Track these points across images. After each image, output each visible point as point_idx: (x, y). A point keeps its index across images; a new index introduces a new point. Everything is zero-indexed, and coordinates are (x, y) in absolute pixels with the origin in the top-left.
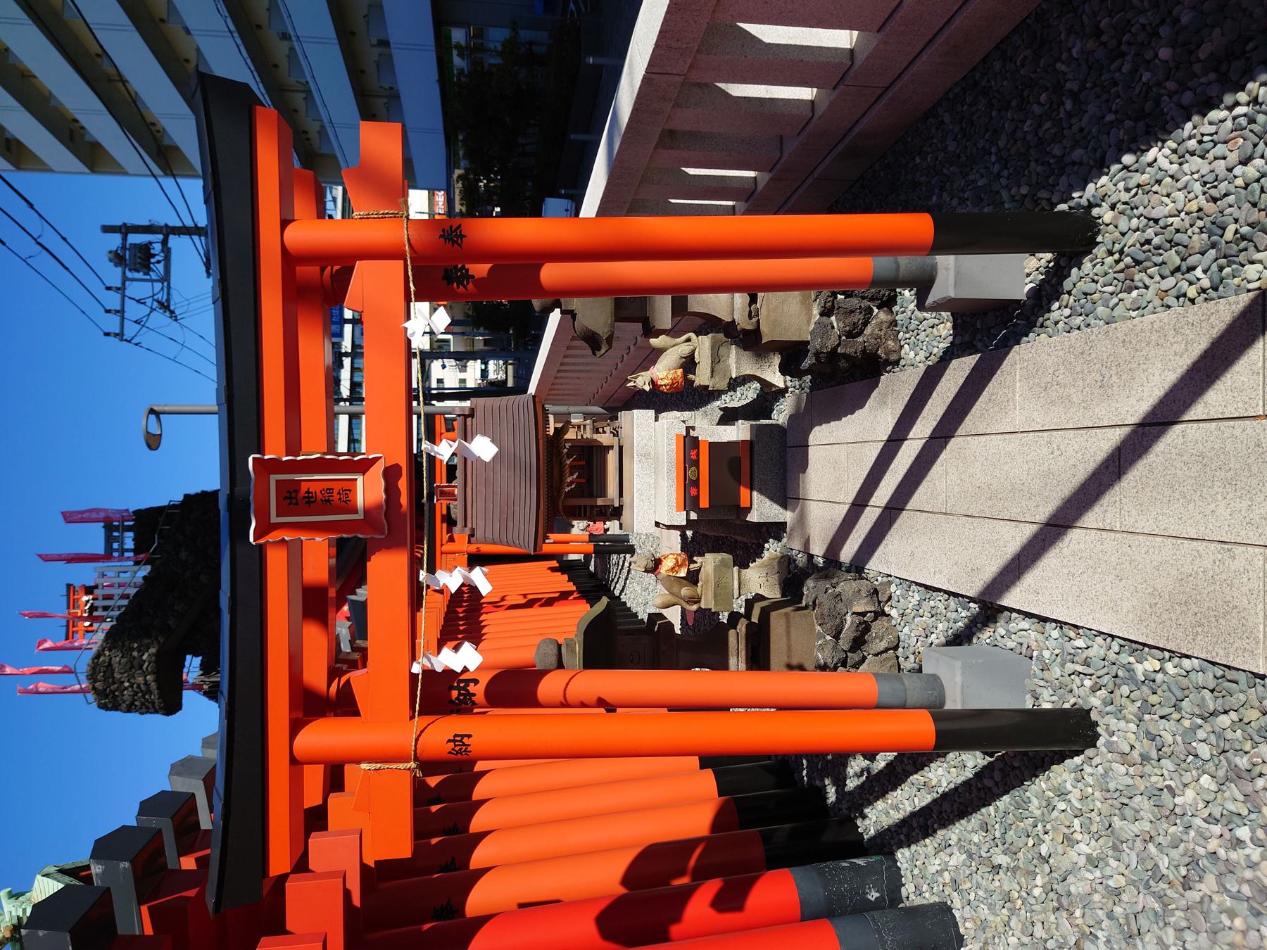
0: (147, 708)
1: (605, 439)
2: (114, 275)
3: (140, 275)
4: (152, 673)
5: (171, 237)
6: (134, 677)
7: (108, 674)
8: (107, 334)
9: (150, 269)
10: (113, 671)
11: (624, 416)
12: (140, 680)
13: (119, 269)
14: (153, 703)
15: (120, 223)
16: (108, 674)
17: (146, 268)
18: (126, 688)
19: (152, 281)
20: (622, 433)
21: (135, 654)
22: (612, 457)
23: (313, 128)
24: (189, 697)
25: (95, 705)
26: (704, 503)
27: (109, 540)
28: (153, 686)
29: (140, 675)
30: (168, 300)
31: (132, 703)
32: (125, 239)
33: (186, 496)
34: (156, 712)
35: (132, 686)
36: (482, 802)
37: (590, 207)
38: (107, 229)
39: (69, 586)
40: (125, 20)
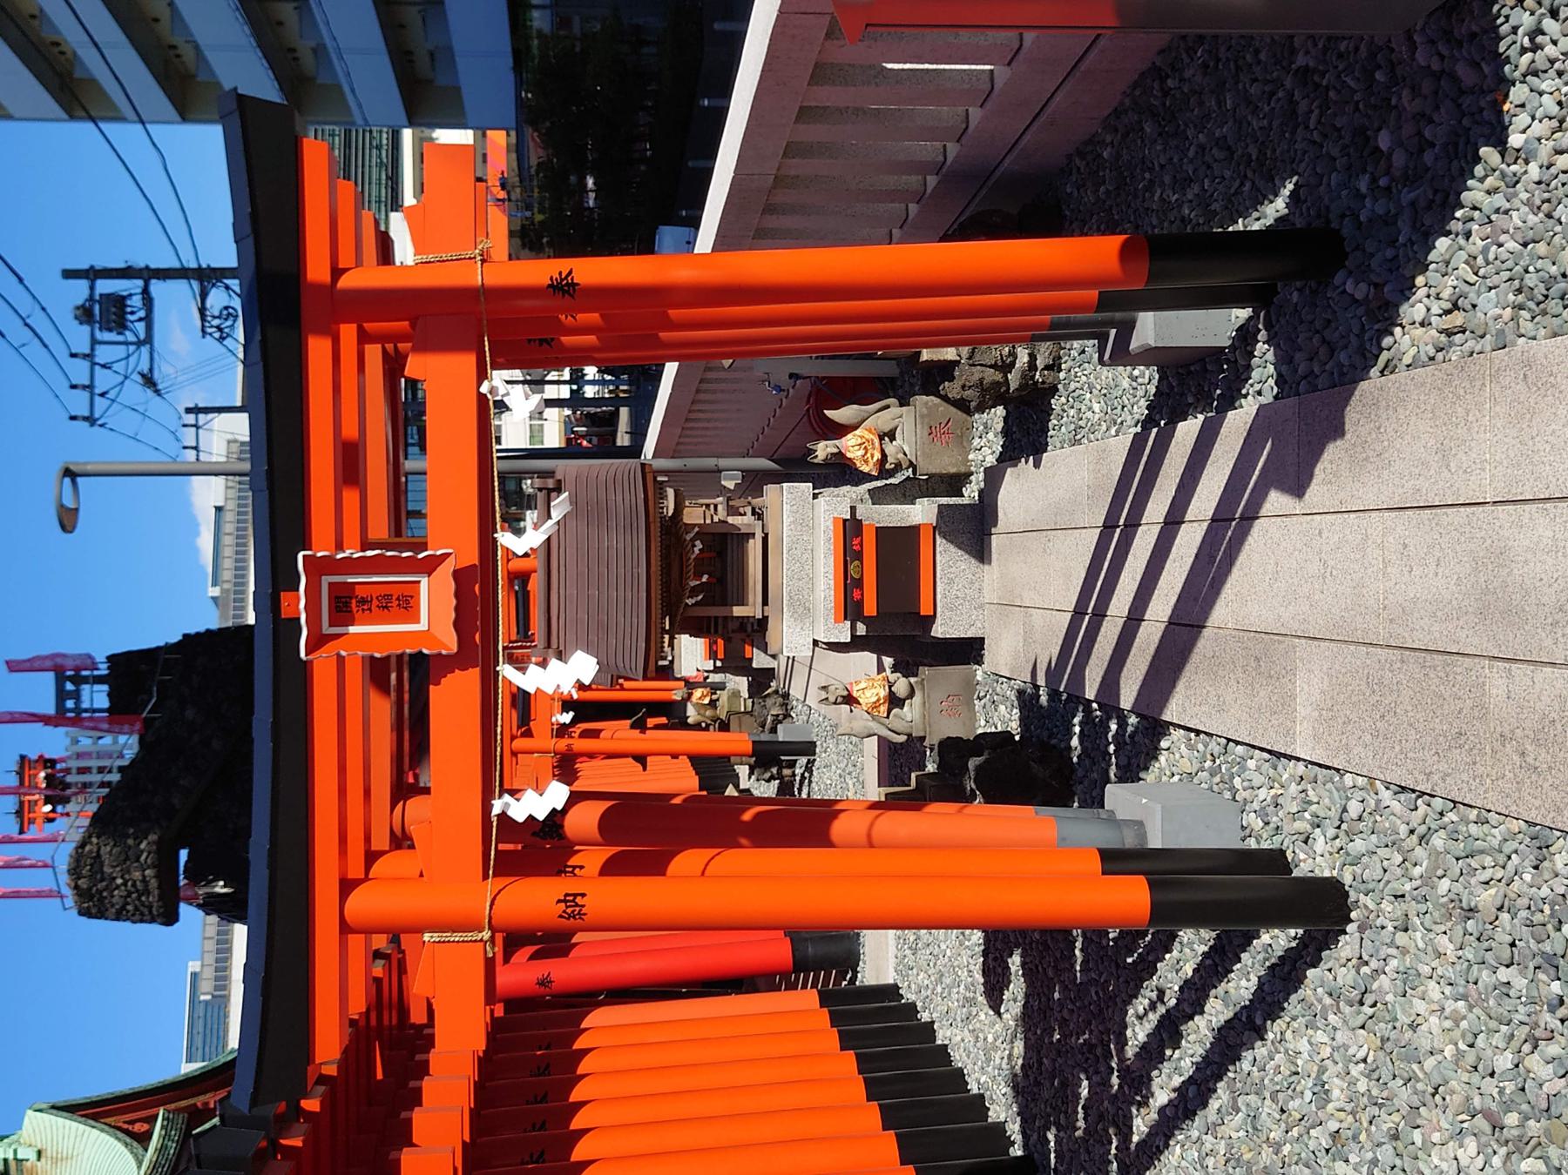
0: (142, 914)
1: (743, 521)
2: (80, 336)
3: (112, 336)
4: (153, 866)
5: (153, 281)
6: (129, 872)
7: (96, 867)
8: (73, 418)
9: (125, 327)
10: (102, 865)
11: (770, 490)
12: (137, 875)
13: (86, 329)
14: (150, 908)
15: (86, 266)
16: (96, 867)
17: (121, 325)
18: (118, 887)
19: (126, 343)
20: (769, 516)
21: (130, 842)
22: (754, 547)
23: (304, 47)
24: (184, 908)
25: (75, 912)
26: (870, 609)
27: (61, 695)
28: (154, 883)
29: (136, 869)
30: (151, 370)
31: (123, 908)
32: (92, 288)
33: (185, 636)
34: (152, 921)
35: (125, 884)
36: (583, 1104)
37: (705, 239)
38: (69, 274)
39: (23, 758)
40: (123, 38)
